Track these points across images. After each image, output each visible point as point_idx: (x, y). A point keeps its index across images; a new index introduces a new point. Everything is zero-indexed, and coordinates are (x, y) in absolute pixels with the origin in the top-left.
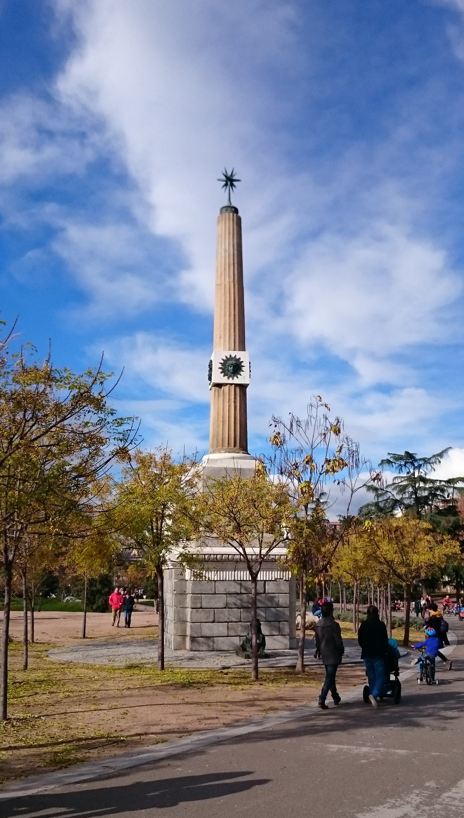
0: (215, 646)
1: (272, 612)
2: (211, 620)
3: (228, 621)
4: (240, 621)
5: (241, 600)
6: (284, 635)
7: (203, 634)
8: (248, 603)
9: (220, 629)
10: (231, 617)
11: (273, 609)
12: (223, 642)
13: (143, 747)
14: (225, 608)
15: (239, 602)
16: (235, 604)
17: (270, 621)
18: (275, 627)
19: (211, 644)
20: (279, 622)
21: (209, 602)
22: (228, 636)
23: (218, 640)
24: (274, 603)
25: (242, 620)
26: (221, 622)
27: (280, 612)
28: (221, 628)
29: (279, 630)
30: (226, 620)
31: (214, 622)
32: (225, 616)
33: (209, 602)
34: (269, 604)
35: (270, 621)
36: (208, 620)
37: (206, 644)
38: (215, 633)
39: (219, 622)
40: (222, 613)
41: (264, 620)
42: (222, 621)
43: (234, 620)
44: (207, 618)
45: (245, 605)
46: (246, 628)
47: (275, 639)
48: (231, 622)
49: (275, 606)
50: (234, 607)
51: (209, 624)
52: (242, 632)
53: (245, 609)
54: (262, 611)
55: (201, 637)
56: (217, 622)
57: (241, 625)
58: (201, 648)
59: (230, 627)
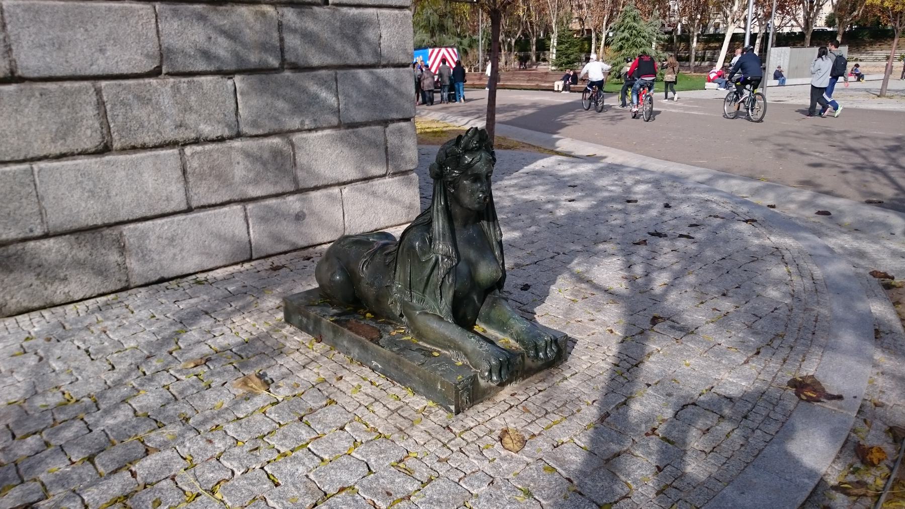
0: (133, 264)
1: (358, 86)
2: (89, 138)
3: (181, 135)
4: (239, 135)
5: (231, 35)
6: (405, 173)
7: (55, 220)
8: (264, 47)
9: (148, 180)
10: (191, 119)
11: (361, 73)
12: (172, 240)
13: (528, 194)
14: (156, 73)
15: (222, 48)
16: (206, 55)
17: (353, 125)
18: (373, 144)
19: (114, 257)
20: (385, 123)
21: (59, 45)
22: (189, 210)
23: (144, 236)
24: (364, 47)
25: (245, 130)
26: (144, 148)
27: (386, 84)
28: (149, 179)
29: (388, 155)
30: (170, 134)
31: (105, 149)
32: (163, 115)
33: (59, 45)
34: (353, 57)
35: (353, 125)
36: (71, 145)
37: (80, 264)
38: (125, 203)
39: (134, 149)
40: (144, 100)
41: (335, 121)
42: (149, 139)
43: (207, 130)
44: (66, 130)
45: (254, 58)
46: (264, 164)
47: (374, 194)
48: (196, 142)
49: (369, 59)
50: (201, 66)
51: (82, 161)
52: (256, 182)
53: (254, 78)
54: (323, 83)
55: (46, 236)
56: (123, 150)
57: (247, 154)
58: (59, 292)
59: (194, 164)
